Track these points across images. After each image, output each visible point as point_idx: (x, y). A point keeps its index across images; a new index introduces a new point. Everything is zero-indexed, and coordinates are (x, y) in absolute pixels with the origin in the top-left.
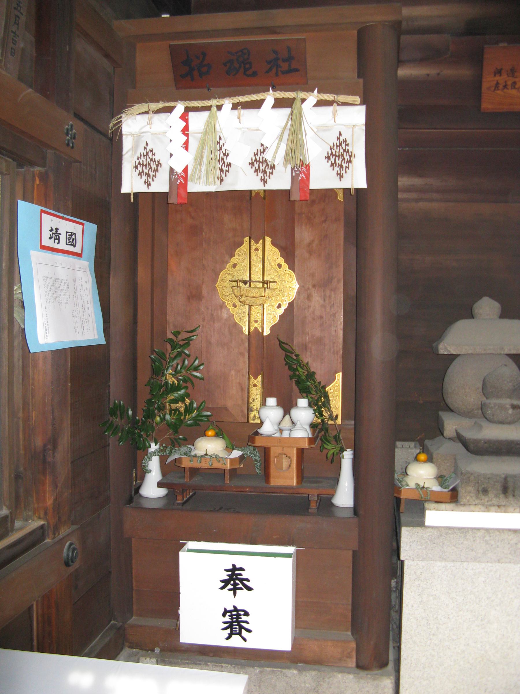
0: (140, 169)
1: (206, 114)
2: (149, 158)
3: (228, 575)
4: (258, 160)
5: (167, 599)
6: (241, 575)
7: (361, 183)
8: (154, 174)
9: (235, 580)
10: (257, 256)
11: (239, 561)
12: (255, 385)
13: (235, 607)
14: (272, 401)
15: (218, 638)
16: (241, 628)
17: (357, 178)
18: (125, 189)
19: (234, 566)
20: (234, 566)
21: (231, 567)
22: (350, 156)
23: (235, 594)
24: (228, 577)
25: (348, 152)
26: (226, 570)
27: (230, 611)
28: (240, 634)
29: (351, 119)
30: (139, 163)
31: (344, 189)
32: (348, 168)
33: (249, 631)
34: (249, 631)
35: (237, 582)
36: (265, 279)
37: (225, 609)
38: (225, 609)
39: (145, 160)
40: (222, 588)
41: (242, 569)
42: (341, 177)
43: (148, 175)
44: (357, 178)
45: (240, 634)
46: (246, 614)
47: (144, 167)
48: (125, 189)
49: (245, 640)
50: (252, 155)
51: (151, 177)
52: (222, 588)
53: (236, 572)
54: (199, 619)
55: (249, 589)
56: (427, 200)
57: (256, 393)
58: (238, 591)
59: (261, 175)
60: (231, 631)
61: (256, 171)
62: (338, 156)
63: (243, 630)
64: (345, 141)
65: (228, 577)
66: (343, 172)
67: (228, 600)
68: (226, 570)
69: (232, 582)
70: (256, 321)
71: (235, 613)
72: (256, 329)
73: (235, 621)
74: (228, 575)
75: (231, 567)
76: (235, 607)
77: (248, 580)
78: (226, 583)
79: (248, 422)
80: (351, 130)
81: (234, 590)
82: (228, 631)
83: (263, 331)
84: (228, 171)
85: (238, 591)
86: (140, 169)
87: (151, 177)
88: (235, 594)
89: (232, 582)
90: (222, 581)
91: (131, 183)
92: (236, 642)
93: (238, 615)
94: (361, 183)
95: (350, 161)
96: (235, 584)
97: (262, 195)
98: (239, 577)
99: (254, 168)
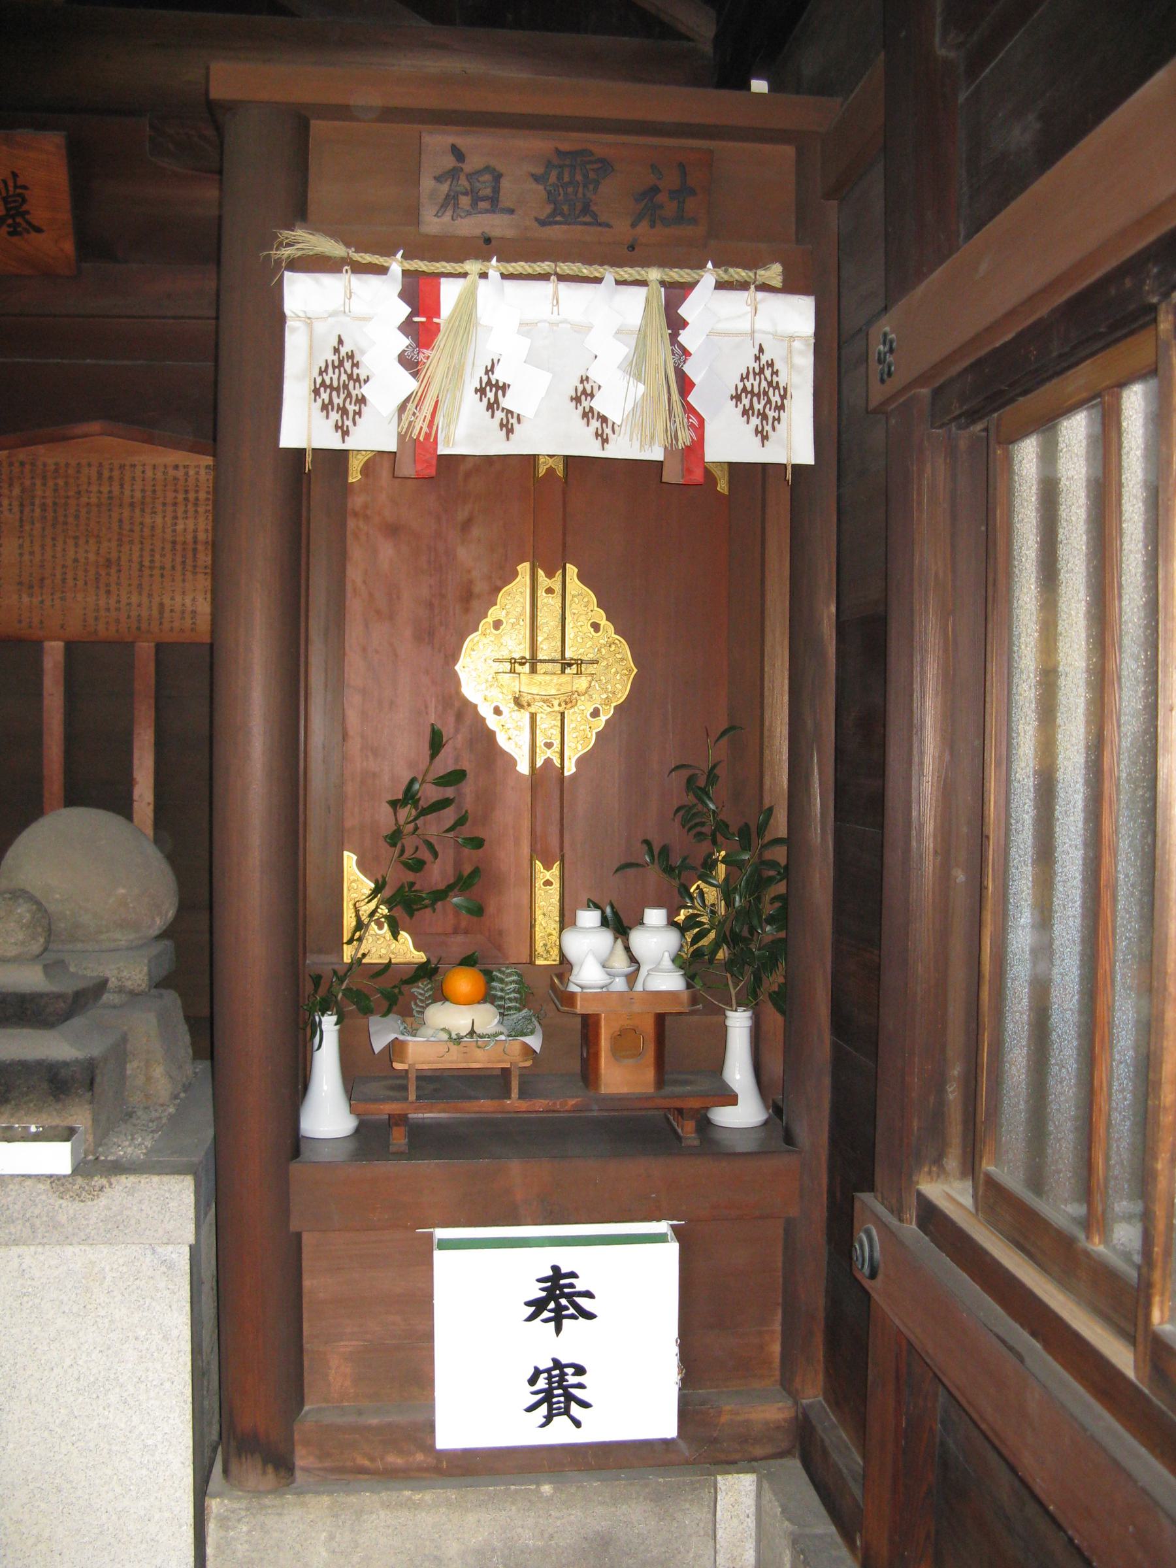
0: (325, 396)
1: (461, 281)
2: (345, 372)
3: (542, 1289)
4: (749, 389)
5: (407, 1364)
6: (572, 1286)
7: (805, 454)
8: (357, 408)
9: (558, 1299)
10: (549, 604)
11: (567, 1257)
12: (548, 883)
13: (555, 1361)
14: (589, 918)
15: (528, 1431)
16: (570, 1398)
17: (795, 442)
18: (291, 436)
19: (555, 1269)
20: (555, 1269)
21: (550, 1273)
22: (783, 397)
23: (558, 1329)
24: (544, 1294)
25: (777, 387)
26: (540, 1280)
27: (548, 1371)
28: (567, 1412)
29: (786, 324)
30: (323, 383)
31: (730, 464)
32: (779, 420)
33: (585, 1405)
34: (585, 1405)
35: (564, 1302)
36: (568, 655)
37: (536, 1369)
38: (536, 1369)
39: (335, 377)
40: (530, 1318)
41: (573, 1275)
42: (765, 438)
43: (344, 411)
44: (795, 442)
45: (567, 1412)
46: (580, 1370)
47: (334, 394)
48: (291, 436)
49: (578, 1424)
50: (737, 380)
51: (351, 414)
52: (530, 1318)
53: (562, 1282)
54: (478, 1396)
55: (590, 1316)
56: (919, 495)
57: (547, 900)
58: (565, 1322)
59: (755, 421)
60: (550, 1409)
61: (745, 412)
62: (759, 396)
63: (573, 1403)
64: (771, 364)
65: (544, 1294)
66: (768, 428)
67: (544, 1344)
68: (540, 1280)
69: (552, 1305)
70: (549, 745)
71: (557, 1372)
72: (548, 761)
73: (557, 1389)
74: (542, 1289)
75: (550, 1273)
76: (555, 1361)
77: (588, 1295)
78: (538, 1305)
79: (532, 963)
80: (786, 344)
81: (558, 1320)
82: (544, 1409)
83: (562, 768)
84: (359, 413)
85: (565, 1322)
86: (325, 396)
87: (351, 414)
88: (558, 1329)
89: (552, 1305)
90: (528, 1304)
91: (302, 426)
92: (561, 1432)
93: (563, 1375)
94: (805, 454)
95: (781, 408)
96: (559, 1309)
97: (560, 472)
98: (566, 1290)
99: (741, 406)
